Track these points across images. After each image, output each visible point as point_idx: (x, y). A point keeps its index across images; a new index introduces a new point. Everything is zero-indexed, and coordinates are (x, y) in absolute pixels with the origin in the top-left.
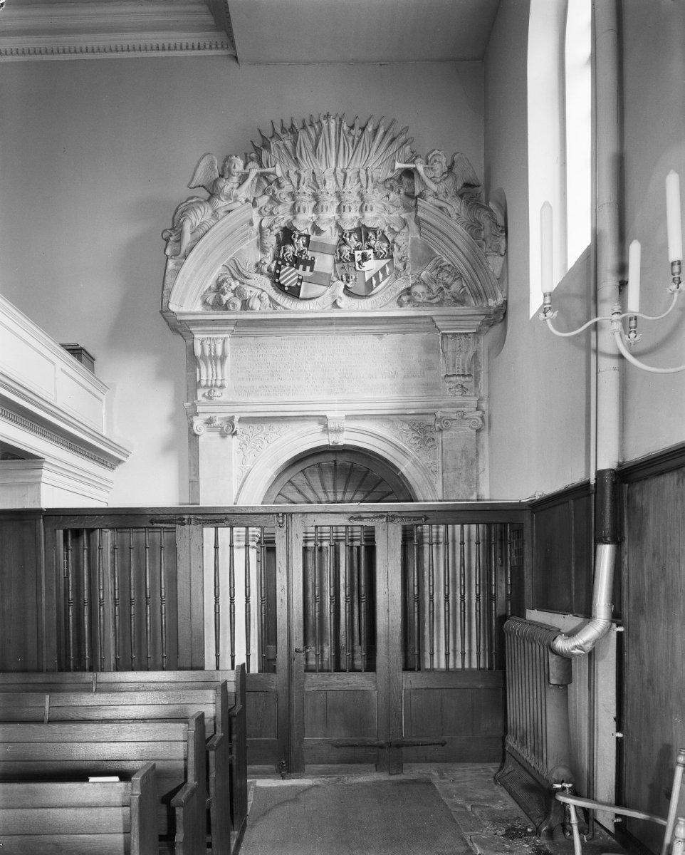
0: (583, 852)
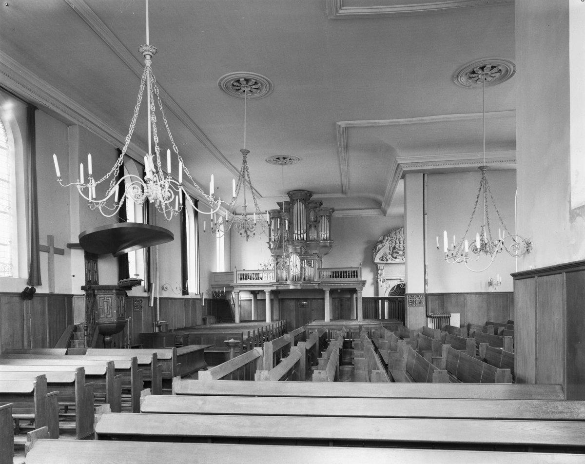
0: (3, 409)
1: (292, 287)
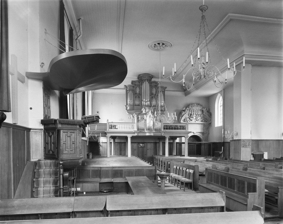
1: (147, 134)
